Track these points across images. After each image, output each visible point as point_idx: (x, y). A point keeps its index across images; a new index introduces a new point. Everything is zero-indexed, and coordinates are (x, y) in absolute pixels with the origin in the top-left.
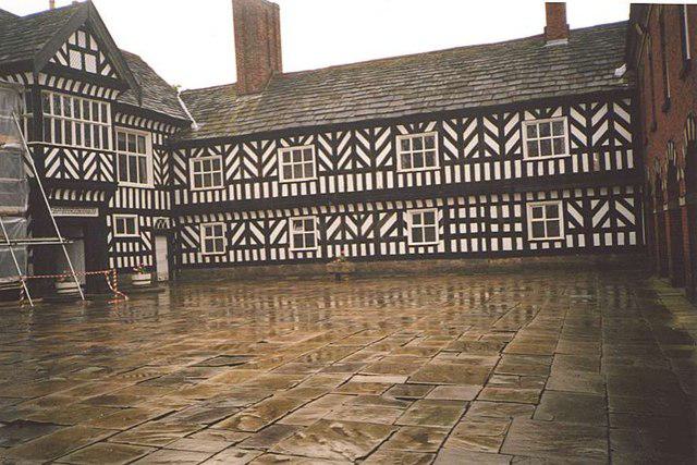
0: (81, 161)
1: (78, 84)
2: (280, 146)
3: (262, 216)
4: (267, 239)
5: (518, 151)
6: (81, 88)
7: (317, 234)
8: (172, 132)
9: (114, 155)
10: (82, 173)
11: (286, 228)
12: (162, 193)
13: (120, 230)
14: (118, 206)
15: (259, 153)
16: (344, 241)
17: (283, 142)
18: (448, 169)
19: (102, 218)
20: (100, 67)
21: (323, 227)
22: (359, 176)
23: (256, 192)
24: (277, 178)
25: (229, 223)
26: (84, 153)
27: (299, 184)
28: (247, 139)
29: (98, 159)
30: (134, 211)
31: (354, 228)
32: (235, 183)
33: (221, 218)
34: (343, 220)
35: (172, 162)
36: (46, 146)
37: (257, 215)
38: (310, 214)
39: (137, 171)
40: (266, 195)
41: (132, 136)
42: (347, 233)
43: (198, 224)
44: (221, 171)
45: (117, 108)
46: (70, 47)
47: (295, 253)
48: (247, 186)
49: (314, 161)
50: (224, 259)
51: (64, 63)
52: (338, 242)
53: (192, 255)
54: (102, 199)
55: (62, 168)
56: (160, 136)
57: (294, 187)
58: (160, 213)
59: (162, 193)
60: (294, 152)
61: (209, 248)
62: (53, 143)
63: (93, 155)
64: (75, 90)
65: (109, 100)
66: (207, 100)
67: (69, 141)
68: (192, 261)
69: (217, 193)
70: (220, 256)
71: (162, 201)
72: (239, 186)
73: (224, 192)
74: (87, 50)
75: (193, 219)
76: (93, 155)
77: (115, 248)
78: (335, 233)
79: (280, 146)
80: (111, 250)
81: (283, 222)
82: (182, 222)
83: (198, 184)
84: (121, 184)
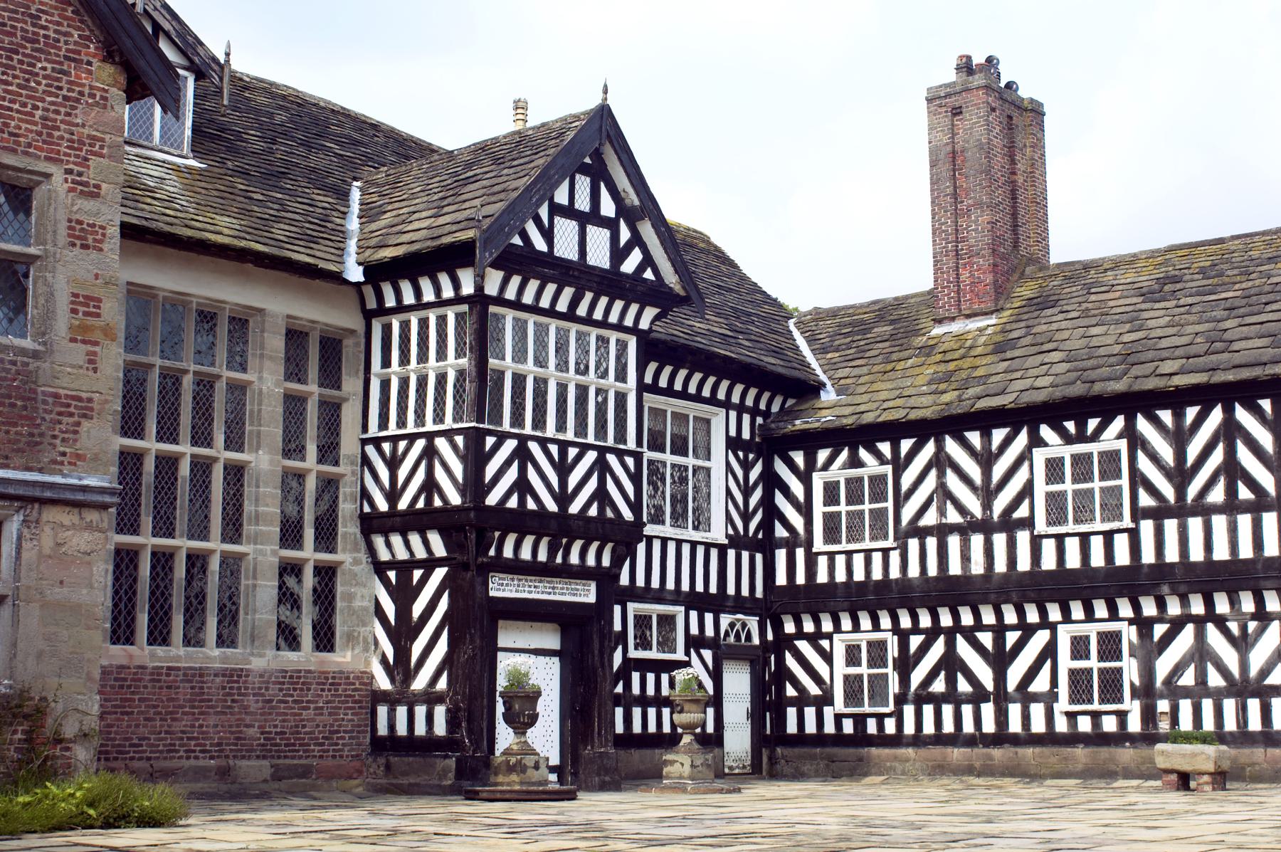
0: (564, 469)
1: (568, 292)
2: (1041, 443)
3: (989, 618)
4: (1000, 678)
5: (1022, 512)
6: (574, 303)
7: (1130, 670)
8: (775, 408)
9: (638, 456)
10: (564, 498)
11: (1050, 652)
12: (745, 555)
13: (644, 644)
14: (640, 582)
15: (986, 460)
16: (1200, 690)
17: (1046, 432)
18: (1147, 527)
19: (601, 611)
20: (619, 254)
21: (1150, 651)
22: (1245, 521)
23: (970, 558)
24: (1029, 523)
25: (904, 636)
26: (573, 452)
27: (1085, 538)
28: (954, 425)
29: (601, 467)
30: (676, 597)
31: (1230, 657)
32: (921, 534)
33: (886, 622)
34: (1200, 636)
35: (772, 482)
36: (490, 433)
37: (977, 615)
38: (1114, 615)
39: (687, 507)
40: (1000, 566)
41: (680, 418)
42: (1211, 669)
43: (829, 636)
44: (890, 504)
45: (651, 349)
46: (555, 210)
47: (1072, 716)
48: (954, 542)
49: (1125, 482)
50: (890, 726)
51: (540, 244)
52: (1186, 692)
53: (810, 712)
54: (606, 562)
55: (522, 486)
56: (746, 418)
57: (1072, 545)
58: (740, 605)
59: (745, 555)
60: (848, 481)
61: (853, 693)
62: (506, 426)
63: (591, 456)
64: (562, 306)
65: (634, 330)
66: (879, 329)
67: (539, 422)
68: (811, 728)
69: (877, 558)
70: (880, 718)
71: (743, 576)
72: (932, 543)
73: (895, 557)
74: (593, 217)
75: (817, 623)
76: (591, 456)
77: (628, 686)
78: (1178, 670)
79: (1041, 443)
80: (619, 689)
81: (1042, 637)
82: (790, 628)
83: (832, 533)
84: (649, 530)
